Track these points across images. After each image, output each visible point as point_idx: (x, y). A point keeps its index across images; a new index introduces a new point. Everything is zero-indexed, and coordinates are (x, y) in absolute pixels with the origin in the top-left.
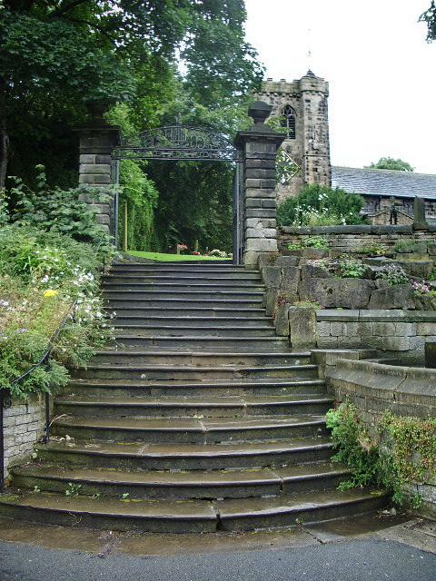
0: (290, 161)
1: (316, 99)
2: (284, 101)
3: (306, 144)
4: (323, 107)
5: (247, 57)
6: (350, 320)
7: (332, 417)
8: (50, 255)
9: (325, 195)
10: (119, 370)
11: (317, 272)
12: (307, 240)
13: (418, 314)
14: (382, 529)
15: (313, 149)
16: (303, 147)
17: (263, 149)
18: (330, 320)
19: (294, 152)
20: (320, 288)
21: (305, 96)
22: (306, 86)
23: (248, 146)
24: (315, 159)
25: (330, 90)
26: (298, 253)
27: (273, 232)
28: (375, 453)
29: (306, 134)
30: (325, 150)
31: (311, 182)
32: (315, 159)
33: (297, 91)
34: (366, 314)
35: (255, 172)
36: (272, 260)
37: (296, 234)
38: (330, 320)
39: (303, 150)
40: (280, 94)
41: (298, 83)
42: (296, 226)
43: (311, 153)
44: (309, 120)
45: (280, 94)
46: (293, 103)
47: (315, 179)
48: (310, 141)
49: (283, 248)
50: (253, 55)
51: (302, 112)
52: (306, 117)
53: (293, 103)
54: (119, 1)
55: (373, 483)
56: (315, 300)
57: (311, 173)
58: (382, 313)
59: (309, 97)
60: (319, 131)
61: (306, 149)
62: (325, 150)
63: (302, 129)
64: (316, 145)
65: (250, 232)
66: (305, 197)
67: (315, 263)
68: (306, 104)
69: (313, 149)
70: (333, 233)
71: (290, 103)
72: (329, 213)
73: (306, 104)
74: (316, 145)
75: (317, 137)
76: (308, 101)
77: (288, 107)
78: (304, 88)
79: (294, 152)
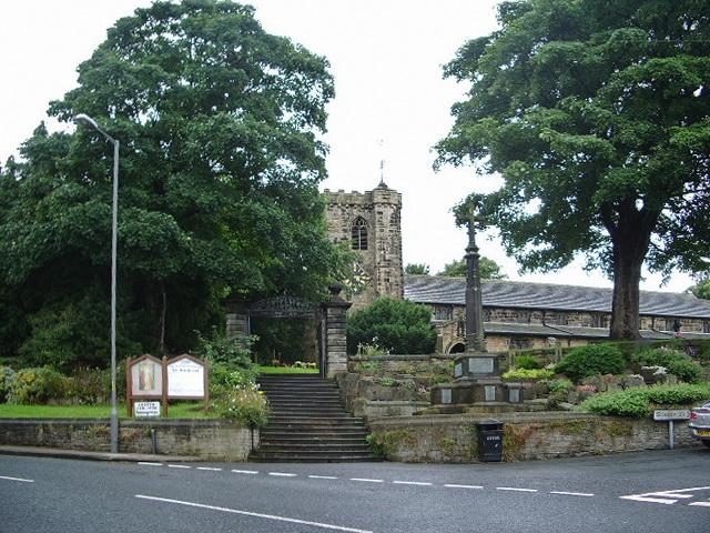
1: (389, 212)
2: (356, 212)
4: (396, 219)
5: (318, 153)
6: (382, 406)
7: (369, 437)
8: (235, 375)
9: (686, 27)
11: (368, 383)
12: (365, 364)
13: (418, 403)
17: (339, 311)
18: (373, 405)
20: (369, 391)
21: (377, 209)
22: (378, 198)
23: (329, 311)
25: (403, 201)
26: (360, 372)
27: (345, 360)
28: (382, 445)
30: (397, 261)
31: (382, 292)
33: (369, 203)
34: (391, 403)
35: (333, 325)
36: (345, 375)
37: (358, 360)
38: (373, 405)
40: (352, 205)
41: (370, 195)
42: (359, 356)
44: (381, 232)
45: (352, 205)
46: (365, 215)
47: (387, 289)
49: (350, 369)
51: (374, 224)
52: (378, 229)
53: (365, 215)
55: (382, 453)
56: (366, 396)
57: (383, 283)
58: (401, 402)
59: (381, 210)
62: (397, 261)
63: (374, 239)
64: (387, 257)
65: (330, 360)
66: (376, 309)
67: (368, 379)
68: (378, 216)
70: (381, 360)
71: (361, 214)
72: (378, 349)
73: (378, 216)
74: (387, 257)
76: (381, 213)
77: (359, 218)
78: (376, 200)
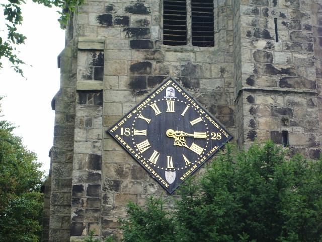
0: (193, 114)
3: (246, 55)
10: (124, 148)
14: (15, 143)
15: (271, 70)
16: (238, 66)
19: (209, 85)
24: (281, 101)
29: (245, 21)
32: (281, 101)
39: (237, 76)
43: (263, 82)
48: (262, 44)
50: (99, 135)
54: (54, 1)
60: (288, 12)
61: (247, 69)
64: (280, 58)
69: (271, 70)
75: (284, 34)
79: (209, 85)
